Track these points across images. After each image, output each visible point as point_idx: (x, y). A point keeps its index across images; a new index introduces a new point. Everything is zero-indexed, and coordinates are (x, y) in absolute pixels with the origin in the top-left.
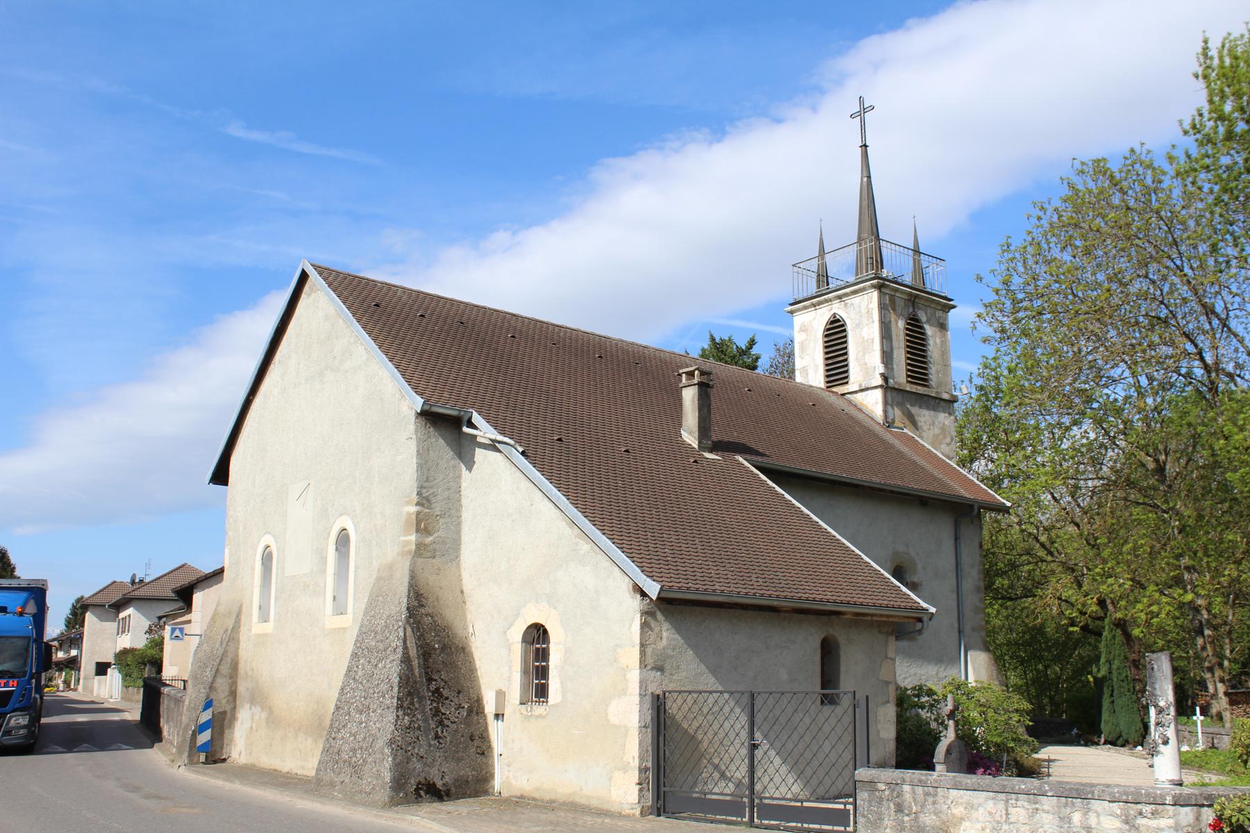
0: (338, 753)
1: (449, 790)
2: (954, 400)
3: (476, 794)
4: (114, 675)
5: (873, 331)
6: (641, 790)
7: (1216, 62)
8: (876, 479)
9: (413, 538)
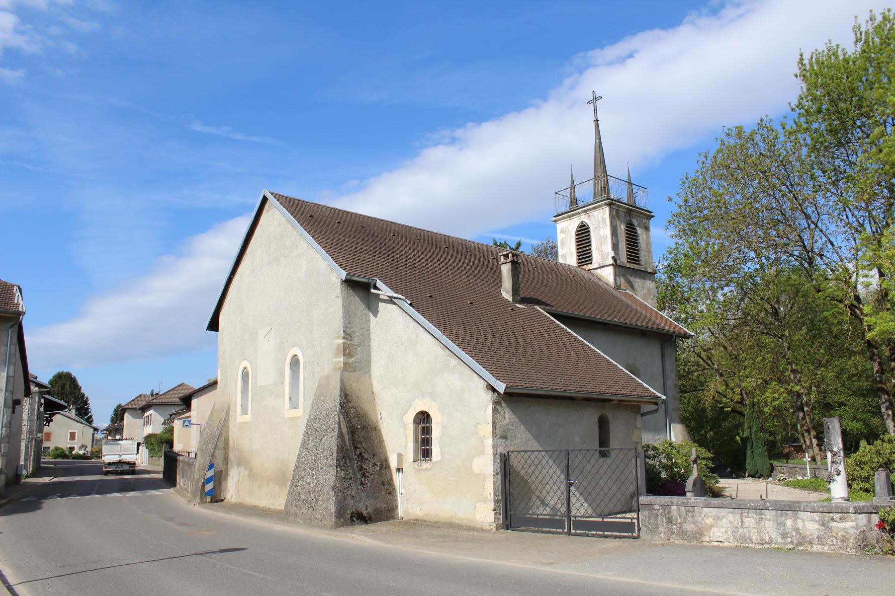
2: (654, 273)
3: (387, 519)
5: (607, 231)
6: (495, 514)
7: (808, 67)
8: (617, 320)
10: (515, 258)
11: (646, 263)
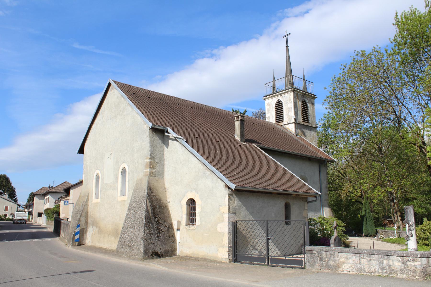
2: (316, 128)
3: (171, 256)
4: (44, 217)
5: (291, 105)
6: (229, 254)
7: (400, 20)
8: (296, 152)
10: (242, 118)
11: (312, 122)
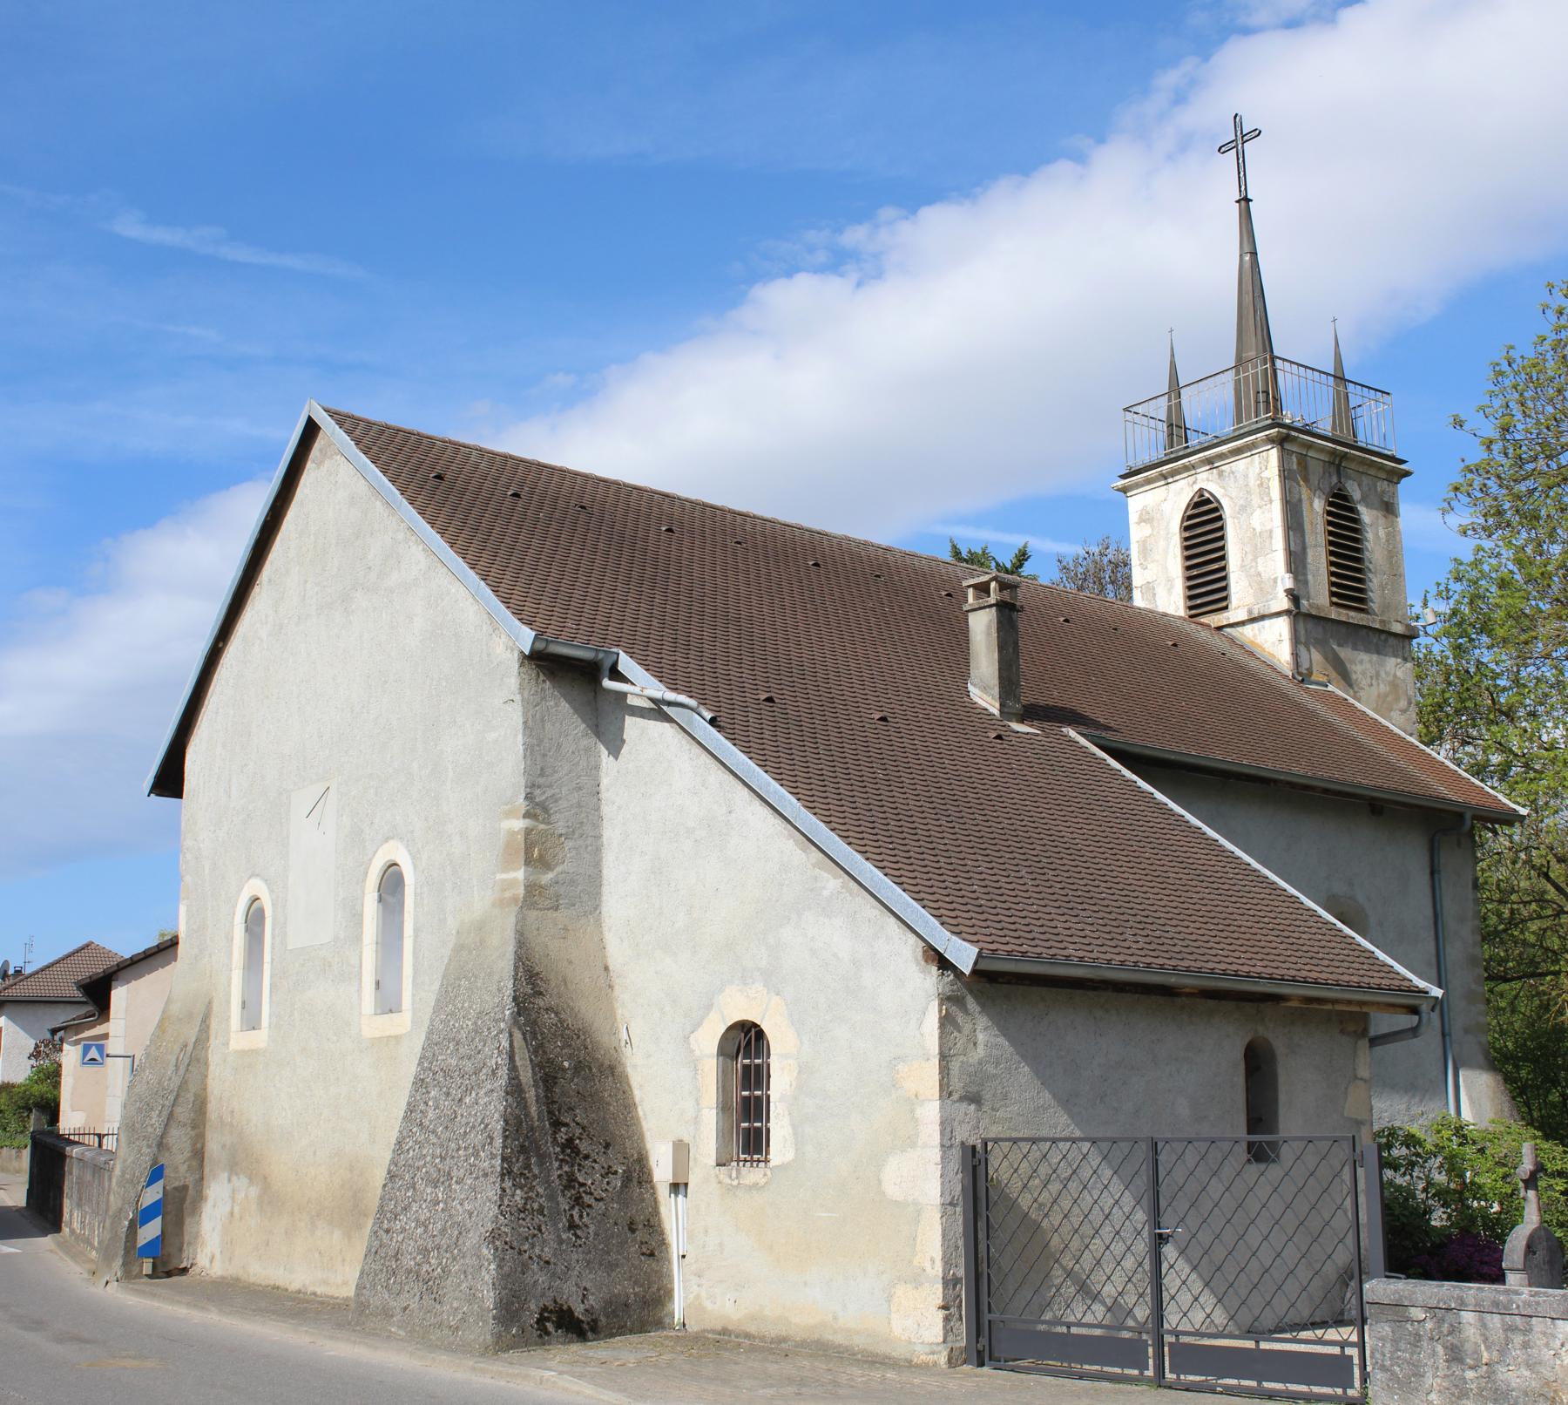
0: (396, 1257)
1: (595, 1321)
2: (1410, 635)
3: (642, 1327)
5: (1272, 517)
6: (947, 1319)
8: (1299, 768)
9: (520, 874)
11: (1386, 607)
